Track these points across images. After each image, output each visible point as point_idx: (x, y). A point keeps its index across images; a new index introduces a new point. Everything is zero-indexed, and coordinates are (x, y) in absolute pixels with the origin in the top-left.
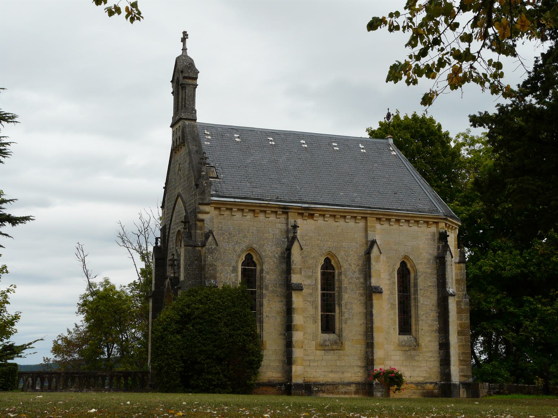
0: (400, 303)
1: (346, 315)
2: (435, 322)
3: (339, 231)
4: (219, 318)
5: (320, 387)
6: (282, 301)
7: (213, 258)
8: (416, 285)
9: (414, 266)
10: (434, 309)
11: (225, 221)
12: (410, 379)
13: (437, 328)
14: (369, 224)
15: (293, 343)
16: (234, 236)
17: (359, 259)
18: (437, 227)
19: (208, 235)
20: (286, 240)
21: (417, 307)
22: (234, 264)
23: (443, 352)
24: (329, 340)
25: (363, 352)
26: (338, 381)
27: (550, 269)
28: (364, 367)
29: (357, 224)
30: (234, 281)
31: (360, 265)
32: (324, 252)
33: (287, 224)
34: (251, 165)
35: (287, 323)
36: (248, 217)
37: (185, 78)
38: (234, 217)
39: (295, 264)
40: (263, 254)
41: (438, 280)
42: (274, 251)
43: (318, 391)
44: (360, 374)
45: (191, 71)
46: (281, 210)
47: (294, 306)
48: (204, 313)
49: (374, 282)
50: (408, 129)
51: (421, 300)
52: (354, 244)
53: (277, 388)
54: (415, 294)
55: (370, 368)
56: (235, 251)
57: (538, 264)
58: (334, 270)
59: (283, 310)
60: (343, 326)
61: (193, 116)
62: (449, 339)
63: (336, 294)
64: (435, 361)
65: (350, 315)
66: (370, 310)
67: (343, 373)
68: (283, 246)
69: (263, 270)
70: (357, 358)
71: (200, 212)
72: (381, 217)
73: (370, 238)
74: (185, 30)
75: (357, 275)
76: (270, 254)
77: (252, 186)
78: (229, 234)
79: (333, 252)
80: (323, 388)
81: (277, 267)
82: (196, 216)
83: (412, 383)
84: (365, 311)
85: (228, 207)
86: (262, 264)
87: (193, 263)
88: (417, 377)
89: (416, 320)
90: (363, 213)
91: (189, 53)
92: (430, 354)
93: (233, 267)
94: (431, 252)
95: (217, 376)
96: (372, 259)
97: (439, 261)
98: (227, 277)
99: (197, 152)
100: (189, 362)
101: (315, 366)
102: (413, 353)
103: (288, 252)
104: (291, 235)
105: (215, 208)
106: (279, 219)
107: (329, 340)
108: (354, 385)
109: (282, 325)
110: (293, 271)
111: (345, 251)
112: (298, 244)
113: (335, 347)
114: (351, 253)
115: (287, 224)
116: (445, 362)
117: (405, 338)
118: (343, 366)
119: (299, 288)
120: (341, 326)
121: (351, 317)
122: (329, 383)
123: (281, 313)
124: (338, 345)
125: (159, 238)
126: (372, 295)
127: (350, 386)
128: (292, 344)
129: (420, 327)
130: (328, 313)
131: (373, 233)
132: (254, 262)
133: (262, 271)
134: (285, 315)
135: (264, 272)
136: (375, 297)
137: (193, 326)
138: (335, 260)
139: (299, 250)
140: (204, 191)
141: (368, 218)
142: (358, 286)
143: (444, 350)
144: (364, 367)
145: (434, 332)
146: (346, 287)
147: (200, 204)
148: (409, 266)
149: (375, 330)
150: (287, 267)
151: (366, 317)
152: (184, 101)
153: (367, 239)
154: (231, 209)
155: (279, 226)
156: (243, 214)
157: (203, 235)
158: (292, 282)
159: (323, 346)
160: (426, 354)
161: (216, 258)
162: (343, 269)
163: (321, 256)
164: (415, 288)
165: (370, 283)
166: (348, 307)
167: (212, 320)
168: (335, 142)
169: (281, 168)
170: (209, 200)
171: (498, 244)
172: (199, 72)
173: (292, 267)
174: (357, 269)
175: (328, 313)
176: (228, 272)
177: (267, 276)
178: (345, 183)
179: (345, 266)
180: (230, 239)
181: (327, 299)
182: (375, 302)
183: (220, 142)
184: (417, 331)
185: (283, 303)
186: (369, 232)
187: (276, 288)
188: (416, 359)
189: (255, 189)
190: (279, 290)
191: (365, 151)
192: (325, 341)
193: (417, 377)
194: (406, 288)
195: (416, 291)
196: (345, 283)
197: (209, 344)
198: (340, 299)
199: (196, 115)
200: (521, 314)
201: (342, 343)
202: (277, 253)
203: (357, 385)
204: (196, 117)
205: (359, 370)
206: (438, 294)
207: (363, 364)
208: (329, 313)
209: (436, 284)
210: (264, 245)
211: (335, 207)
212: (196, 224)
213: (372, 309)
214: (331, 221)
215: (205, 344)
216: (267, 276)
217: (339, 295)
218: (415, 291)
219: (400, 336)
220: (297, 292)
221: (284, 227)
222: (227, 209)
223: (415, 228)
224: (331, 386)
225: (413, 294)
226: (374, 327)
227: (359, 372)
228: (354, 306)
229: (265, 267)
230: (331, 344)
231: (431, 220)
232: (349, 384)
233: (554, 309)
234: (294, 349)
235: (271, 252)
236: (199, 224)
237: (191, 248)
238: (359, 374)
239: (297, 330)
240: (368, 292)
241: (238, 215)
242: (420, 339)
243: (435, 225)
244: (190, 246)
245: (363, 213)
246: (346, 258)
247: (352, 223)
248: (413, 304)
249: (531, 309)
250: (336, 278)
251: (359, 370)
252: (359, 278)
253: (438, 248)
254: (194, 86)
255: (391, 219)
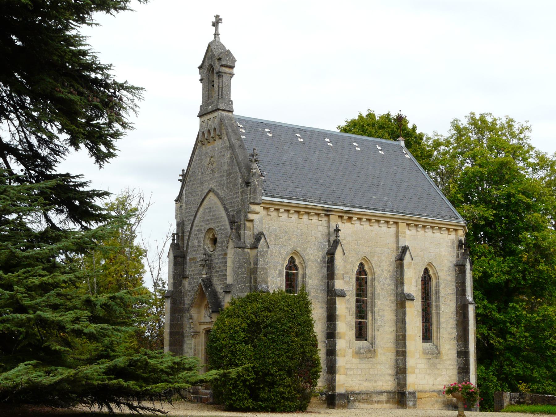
0: (423, 310)
1: (379, 323)
2: (454, 330)
3: (373, 235)
4: (291, 328)
5: (356, 396)
6: (323, 307)
7: (264, 262)
8: (437, 292)
9: (436, 274)
10: (453, 317)
11: (272, 222)
12: (433, 387)
13: (456, 336)
14: (400, 230)
15: (337, 352)
16: (280, 238)
17: (391, 265)
18: (457, 235)
19: (259, 237)
20: (327, 243)
21: (438, 314)
22: (279, 268)
23: (461, 360)
24: (363, 348)
25: (393, 360)
26: (371, 389)
27: (535, 277)
28: (394, 375)
29: (389, 229)
30: (279, 285)
31: (391, 270)
32: (360, 257)
33: (329, 227)
34: (288, 163)
35: (327, 329)
36: (292, 219)
37: (223, 66)
38: (280, 217)
39: (338, 270)
40: (306, 258)
41: (456, 287)
42: (316, 255)
43: (354, 400)
44: (390, 383)
45: (229, 59)
46: (324, 212)
47: (338, 313)
48: (275, 322)
49: (407, 289)
50: (384, 128)
51: (443, 307)
52: (386, 249)
53: (318, 397)
54: (436, 302)
55: (401, 376)
56: (281, 254)
57: (523, 272)
58: (366, 275)
59: (324, 316)
60: (376, 333)
61: (230, 108)
62: (468, 348)
63: (369, 300)
64: (453, 369)
65: (382, 322)
66: (402, 318)
67: (376, 381)
68: (324, 249)
69: (306, 275)
70: (388, 366)
71: (249, 212)
72: (411, 222)
73: (402, 244)
74: (218, 14)
75: (388, 281)
76: (312, 258)
77: (295, 186)
78: (276, 236)
79: (368, 257)
80: (359, 397)
81: (319, 272)
82: (246, 216)
83: (434, 391)
84: (395, 318)
85: (276, 207)
86: (304, 268)
87: (242, 265)
88: (439, 385)
89: (437, 328)
90: (432, 223)
91: (224, 40)
92: (449, 362)
93: (279, 270)
94: (451, 259)
95: (289, 388)
96: (404, 265)
97: (459, 268)
98: (273, 281)
99: (240, 146)
100: (261, 374)
101: (351, 375)
102: (435, 361)
103: (329, 256)
104: (332, 239)
105: (264, 208)
106: (320, 222)
107: (363, 348)
108: (385, 394)
109: (323, 332)
110: (336, 276)
111: (378, 257)
112: (341, 249)
113: (369, 355)
114: (383, 258)
115: (329, 227)
116: (464, 370)
117: (427, 345)
118: (376, 375)
119: (343, 295)
120: (374, 333)
121: (383, 324)
122: (364, 392)
123: (322, 319)
124: (372, 351)
125: (176, 234)
126: (405, 302)
127: (382, 395)
128: (335, 352)
129: (441, 335)
130: (361, 320)
131: (403, 238)
132: (364, 271)
133: (304, 275)
134: (325, 321)
135: (307, 277)
136: (408, 304)
137: (265, 336)
138: (369, 265)
139: (342, 255)
140: (255, 190)
141: (399, 223)
142: (389, 293)
143: (463, 358)
144: (394, 375)
145: (453, 340)
146: (379, 294)
147: (251, 203)
148: (431, 273)
149: (407, 338)
150: (327, 272)
151: (396, 325)
152: (221, 91)
153: (398, 244)
154: (278, 210)
155: (320, 228)
156: (288, 215)
157: (252, 236)
158: (335, 288)
159: (358, 354)
160: (446, 362)
161: (267, 262)
162: (376, 275)
163: (357, 261)
164: (437, 295)
165: (403, 290)
166: (380, 314)
167: (284, 329)
168: (355, 142)
169: (315, 167)
170: (260, 199)
171: (481, 250)
172: (236, 61)
173: (335, 272)
174: (389, 275)
175: (361, 320)
176: (274, 276)
177: (310, 281)
178: (374, 186)
179: (378, 271)
180: (277, 242)
181: (360, 305)
182: (408, 310)
183: (254, 136)
184: (438, 338)
185: (323, 310)
186: (400, 238)
187: (317, 293)
188: (438, 367)
189: (298, 189)
190: (320, 295)
191: (383, 153)
192: (360, 349)
193: (439, 385)
194: (428, 295)
195: (438, 298)
196: (378, 290)
197: (282, 355)
198: (373, 305)
199: (232, 107)
200: (507, 320)
201: (375, 351)
202: (318, 257)
203: (388, 394)
204: (232, 109)
205: (390, 379)
206: (457, 302)
207: (394, 372)
208: (362, 320)
209: (454, 292)
210: (307, 248)
211: (372, 211)
212: (245, 224)
213: (405, 316)
214: (366, 225)
215: (278, 355)
216: (310, 281)
217: (372, 302)
218: (436, 298)
219: (424, 344)
220: (341, 298)
221: (325, 230)
222: (275, 209)
223: (437, 234)
224: (366, 395)
225: (434, 301)
226: (407, 335)
227: (390, 380)
228: (386, 314)
229: (308, 271)
230: (365, 352)
231: (303, 210)
232: (381, 393)
233: (540, 316)
234: (337, 358)
235: (314, 256)
236: (248, 224)
237: (240, 249)
238: (390, 382)
239: (340, 338)
240: (398, 299)
241: (284, 216)
242: (441, 347)
243: (454, 233)
244: (240, 248)
245: (432, 223)
246: (379, 264)
247: (384, 227)
248: (434, 311)
249: (517, 316)
250: (369, 283)
251: (390, 379)
252: (390, 285)
253: (457, 256)
254: (231, 76)
255: (418, 225)
